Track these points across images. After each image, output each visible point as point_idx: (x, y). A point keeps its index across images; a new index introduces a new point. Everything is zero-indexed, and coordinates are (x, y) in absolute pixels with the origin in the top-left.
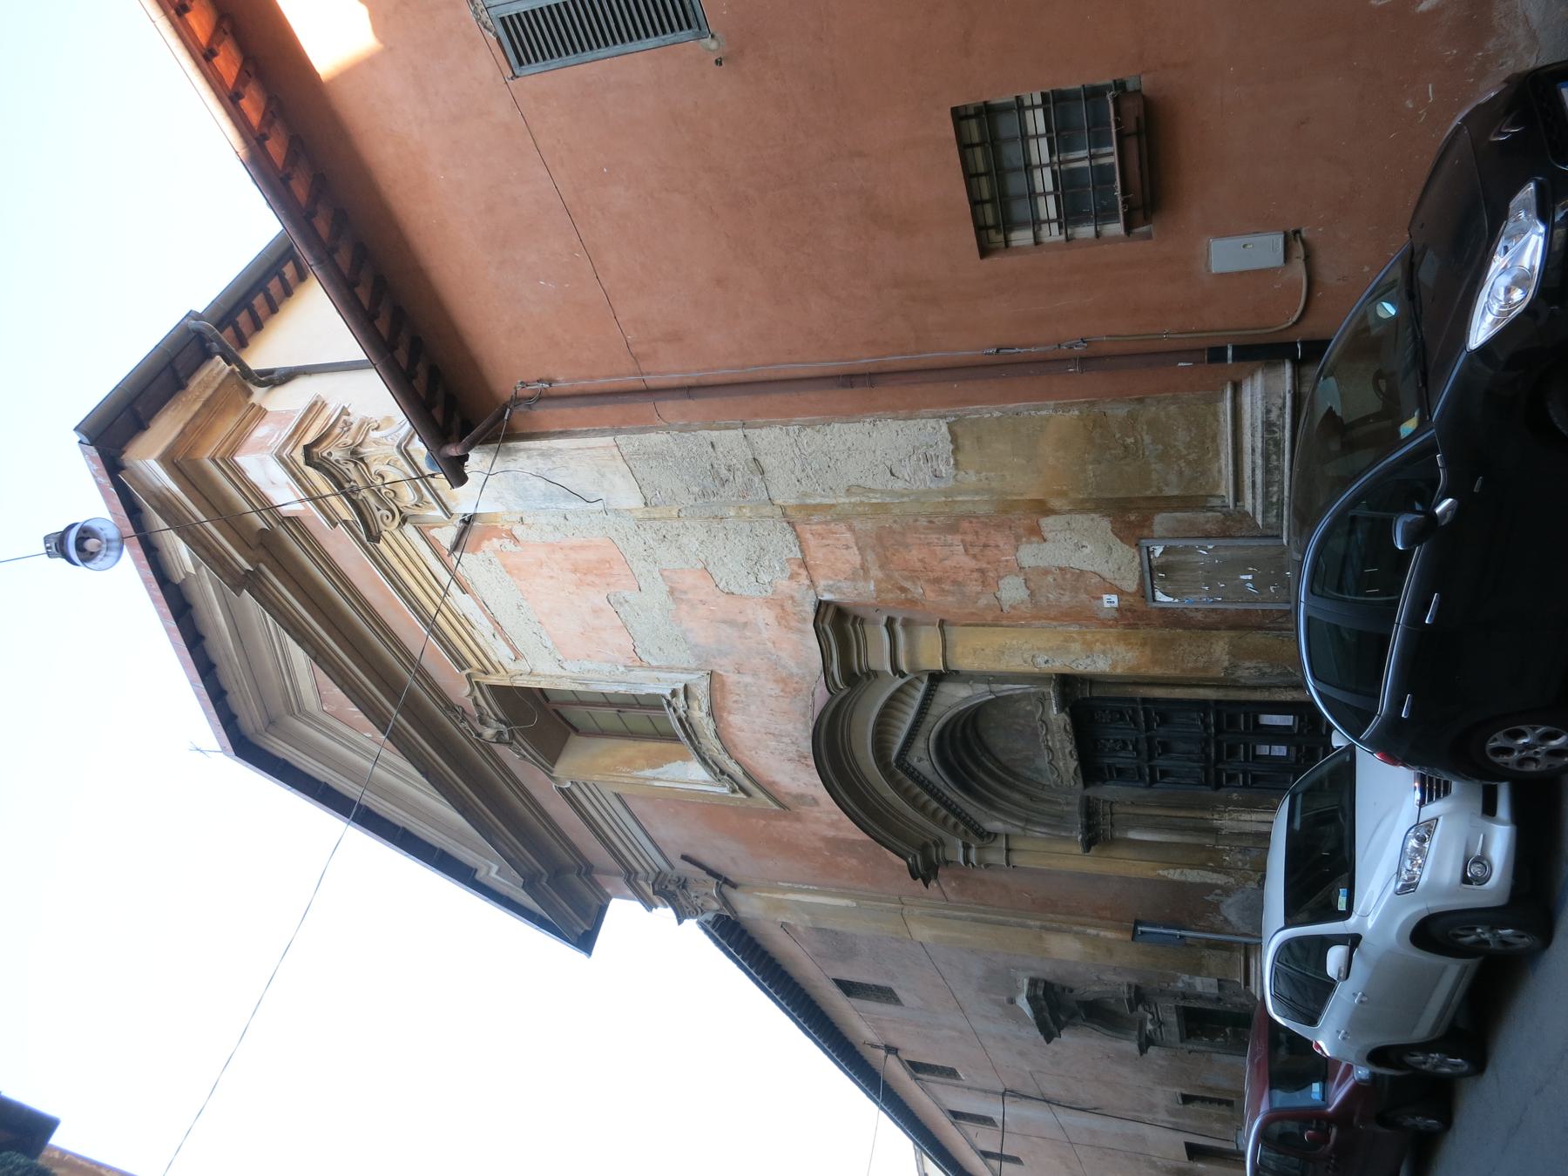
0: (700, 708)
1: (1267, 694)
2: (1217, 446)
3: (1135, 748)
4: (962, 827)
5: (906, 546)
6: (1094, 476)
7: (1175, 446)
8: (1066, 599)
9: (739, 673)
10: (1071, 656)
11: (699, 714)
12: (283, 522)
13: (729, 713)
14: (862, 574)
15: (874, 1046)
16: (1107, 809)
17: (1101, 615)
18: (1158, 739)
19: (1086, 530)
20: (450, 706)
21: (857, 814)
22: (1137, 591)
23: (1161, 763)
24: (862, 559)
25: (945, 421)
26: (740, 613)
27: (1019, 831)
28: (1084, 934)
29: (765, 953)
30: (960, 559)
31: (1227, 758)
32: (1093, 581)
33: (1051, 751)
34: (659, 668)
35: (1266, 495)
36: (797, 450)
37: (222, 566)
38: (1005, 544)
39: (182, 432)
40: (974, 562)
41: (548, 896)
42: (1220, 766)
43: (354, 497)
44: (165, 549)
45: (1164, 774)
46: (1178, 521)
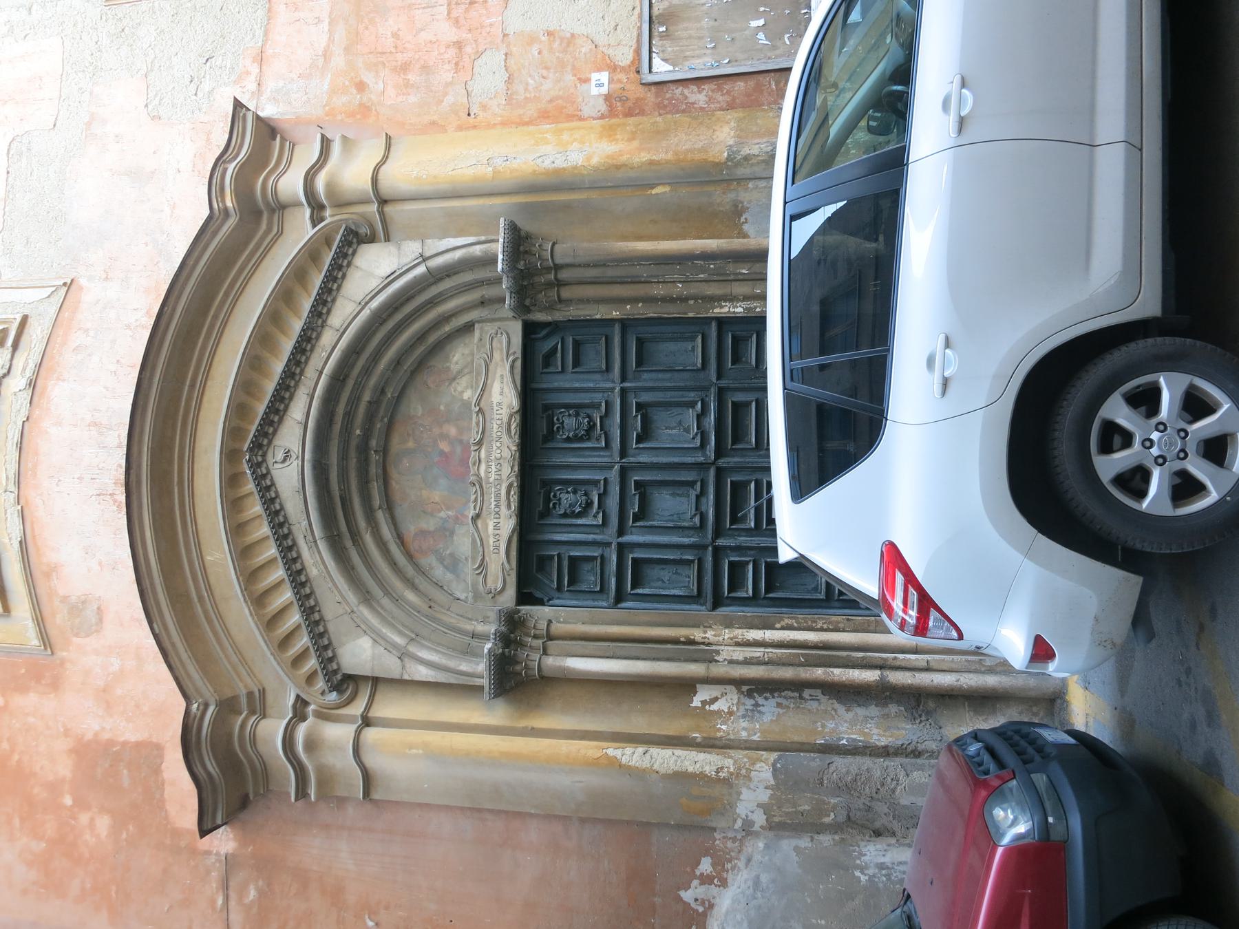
8: (547, 85)
24: (329, 39)
32: (583, 50)
40: (454, 29)
42: (721, 542)
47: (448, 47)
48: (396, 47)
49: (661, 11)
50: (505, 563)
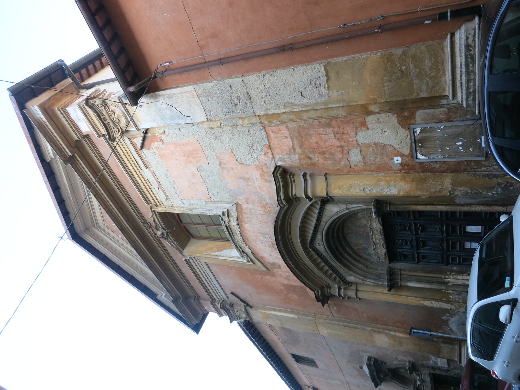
0: (234, 221)
1: (469, 208)
2: (444, 68)
3: (411, 244)
4: (338, 279)
5: (310, 135)
6: (388, 89)
7: (425, 69)
9: (247, 203)
10: (380, 188)
11: (233, 224)
12: (84, 138)
13: (245, 223)
14: (293, 151)
15: (308, 387)
16: (399, 272)
17: (394, 168)
18: (421, 239)
19: (386, 122)
20: (145, 222)
21: (294, 270)
22: (409, 154)
23: (422, 251)
24: (293, 143)
25: (322, 64)
26: (246, 173)
27: (361, 281)
28: (390, 334)
29: (265, 340)
30: (333, 141)
31: (451, 249)
32: (390, 149)
33: (374, 243)
34: (218, 202)
35: (468, 88)
36: (263, 86)
37: (61, 153)
38: (351, 132)
39: (50, 98)
40: (338, 142)
41: (182, 306)
42: (448, 253)
43: (105, 122)
44: (43, 146)
45: (424, 257)
46: (427, 114)
47: (338, 147)
48: (318, 147)
49: (419, 138)
50: (385, 257)
